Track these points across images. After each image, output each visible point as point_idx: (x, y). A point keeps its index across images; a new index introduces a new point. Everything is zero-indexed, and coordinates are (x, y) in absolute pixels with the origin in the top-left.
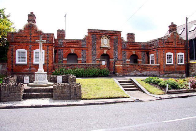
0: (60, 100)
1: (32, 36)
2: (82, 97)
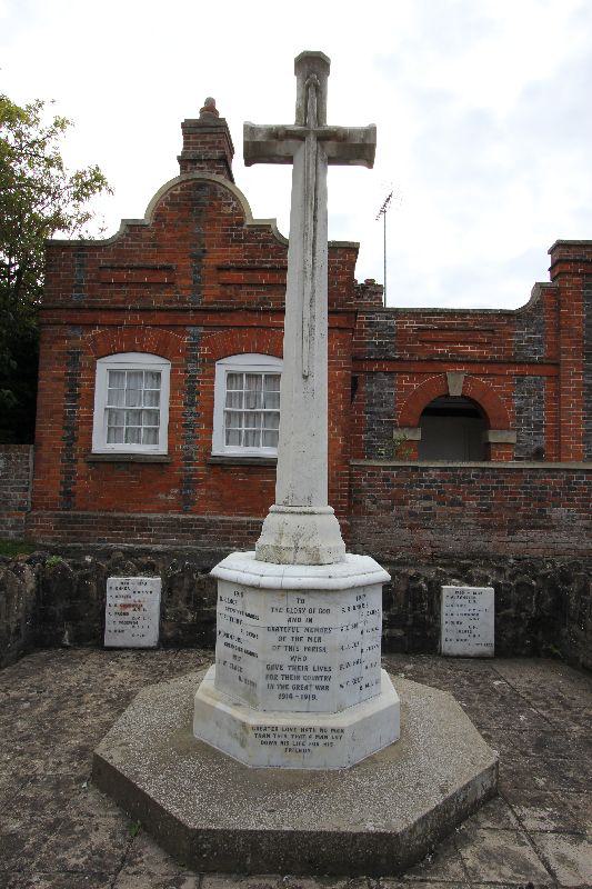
1: (215, 257)
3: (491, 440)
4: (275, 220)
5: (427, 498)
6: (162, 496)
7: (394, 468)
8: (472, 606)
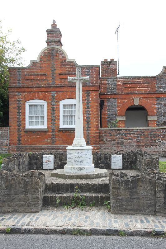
0: (128, 214)
1: (57, 72)
2: (43, 169)
3: (149, 119)
4: (75, 59)
5: (122, 138)
6: (46, 140)
7: (112, 130)
8: (118, 159)
